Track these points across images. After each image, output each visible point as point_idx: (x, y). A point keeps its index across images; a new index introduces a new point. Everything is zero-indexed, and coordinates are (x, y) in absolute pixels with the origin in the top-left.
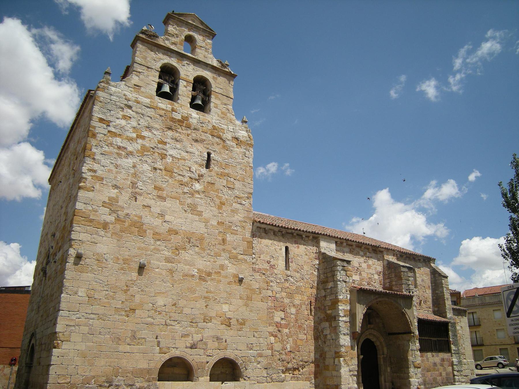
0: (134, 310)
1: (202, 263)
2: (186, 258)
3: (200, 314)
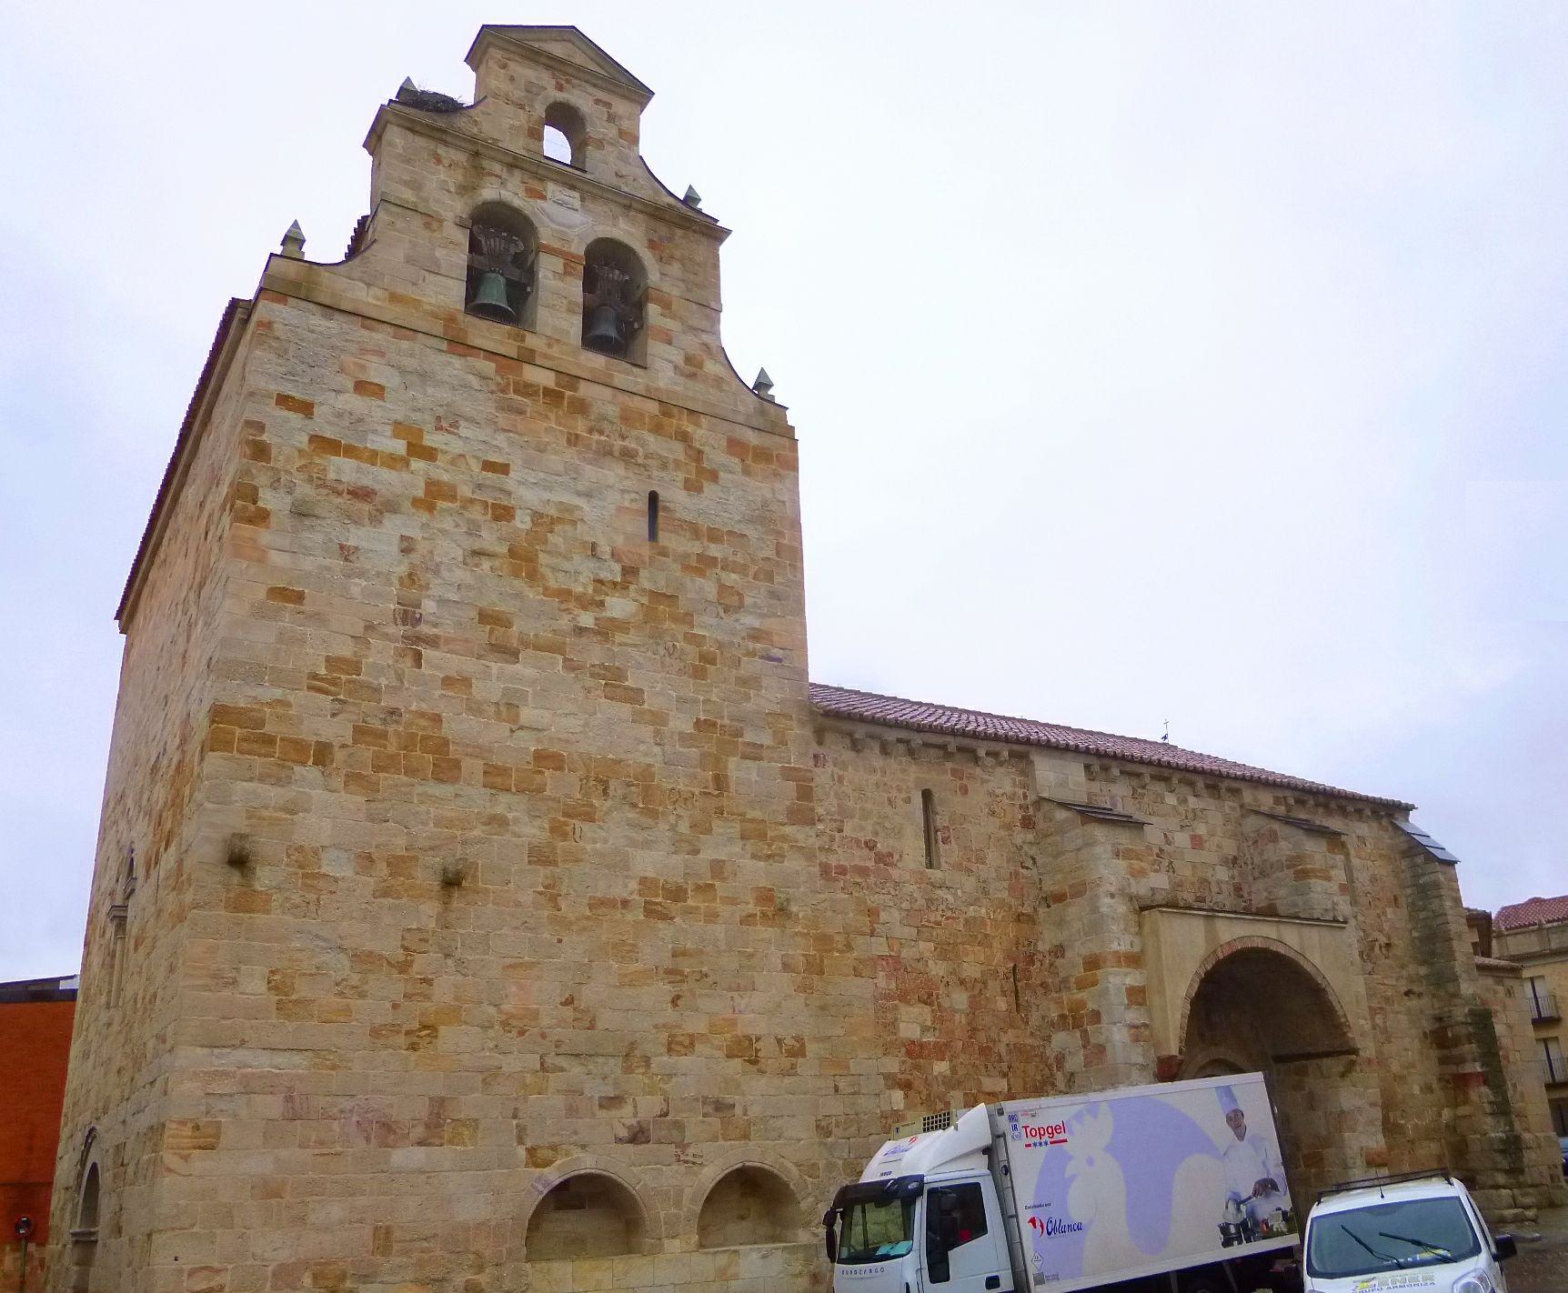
1: (655, 861)
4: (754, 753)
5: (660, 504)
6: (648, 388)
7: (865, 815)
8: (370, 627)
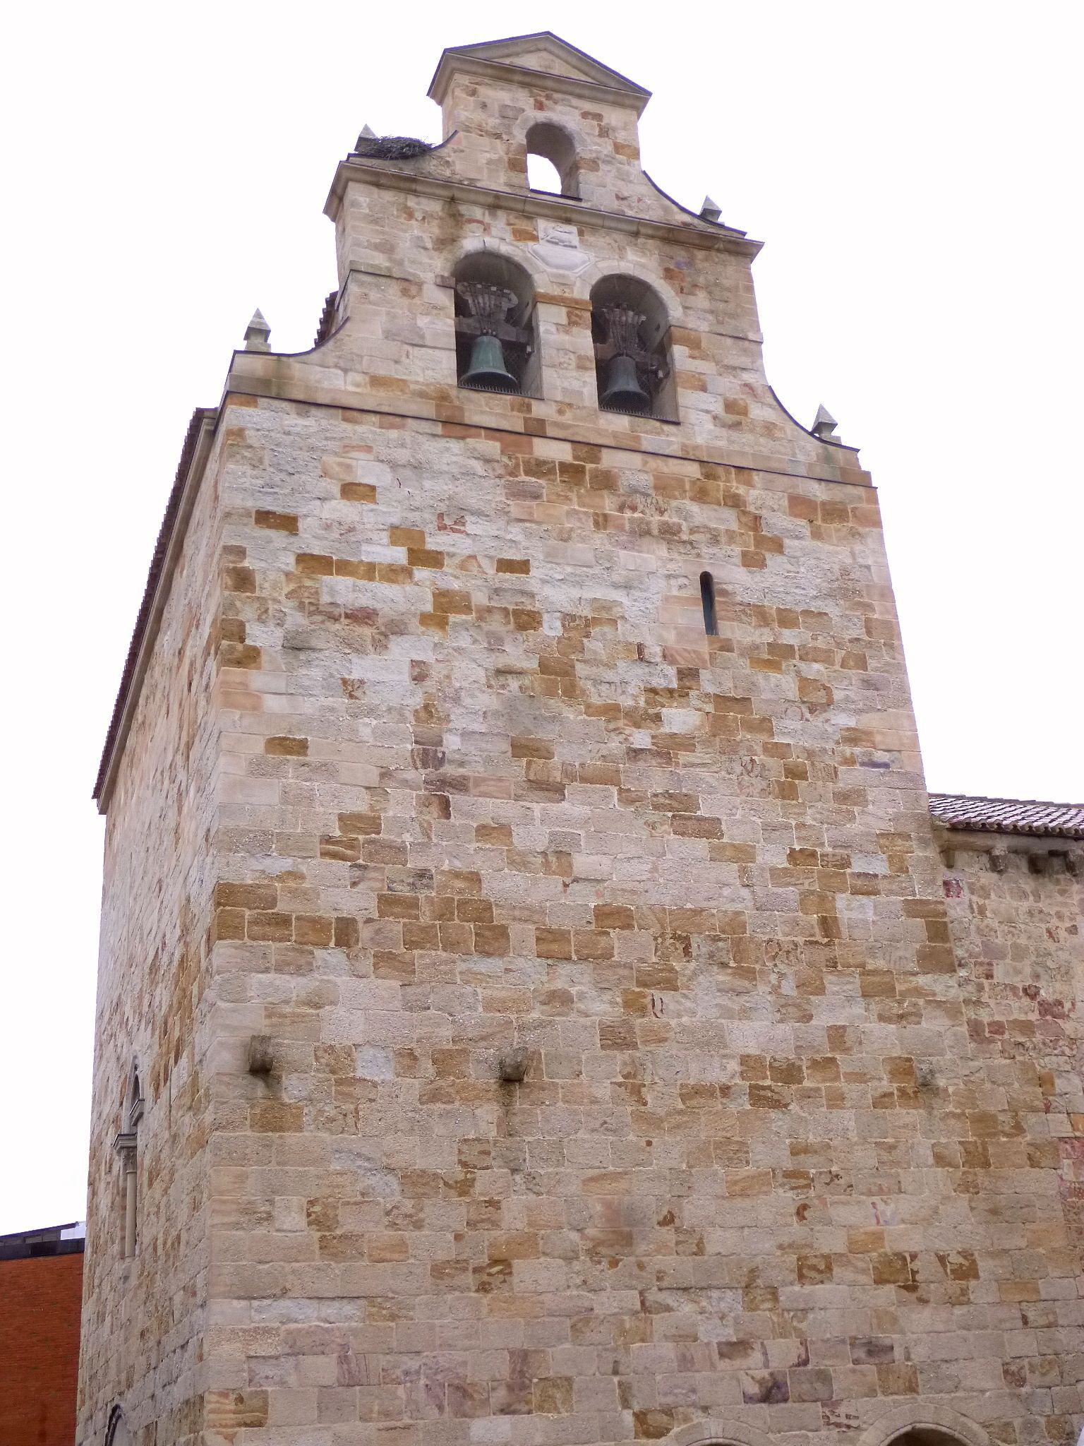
0: (502, 1263)
1: (760, 1032)
2: (685, 1019)
3: (781, 1247)
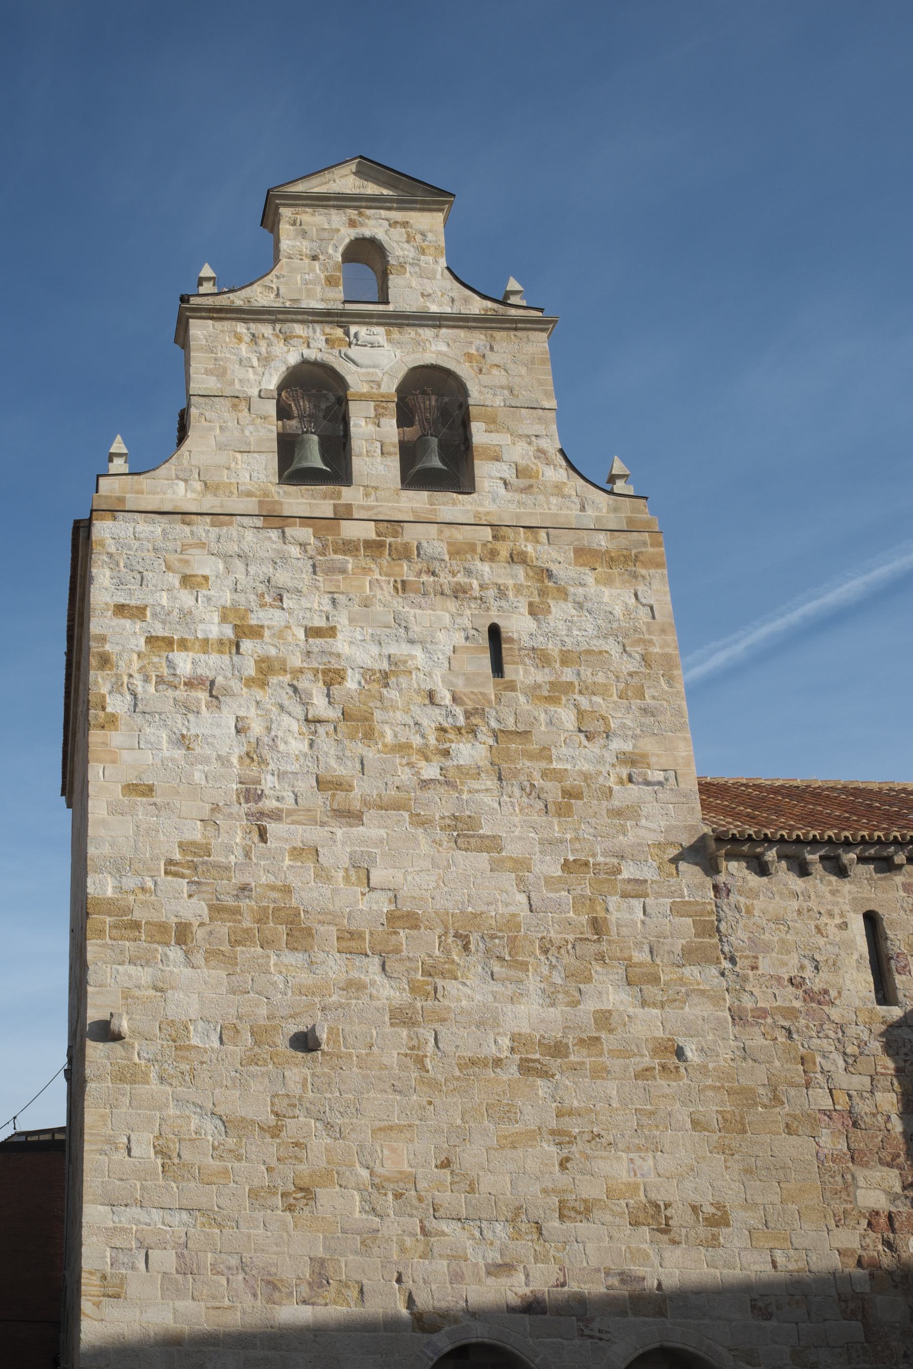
1: (530, 1012)
4: (637, 889)
5: (504, 635)
6: (477, 514)
7: (785, 948)
8: (216, 808)
